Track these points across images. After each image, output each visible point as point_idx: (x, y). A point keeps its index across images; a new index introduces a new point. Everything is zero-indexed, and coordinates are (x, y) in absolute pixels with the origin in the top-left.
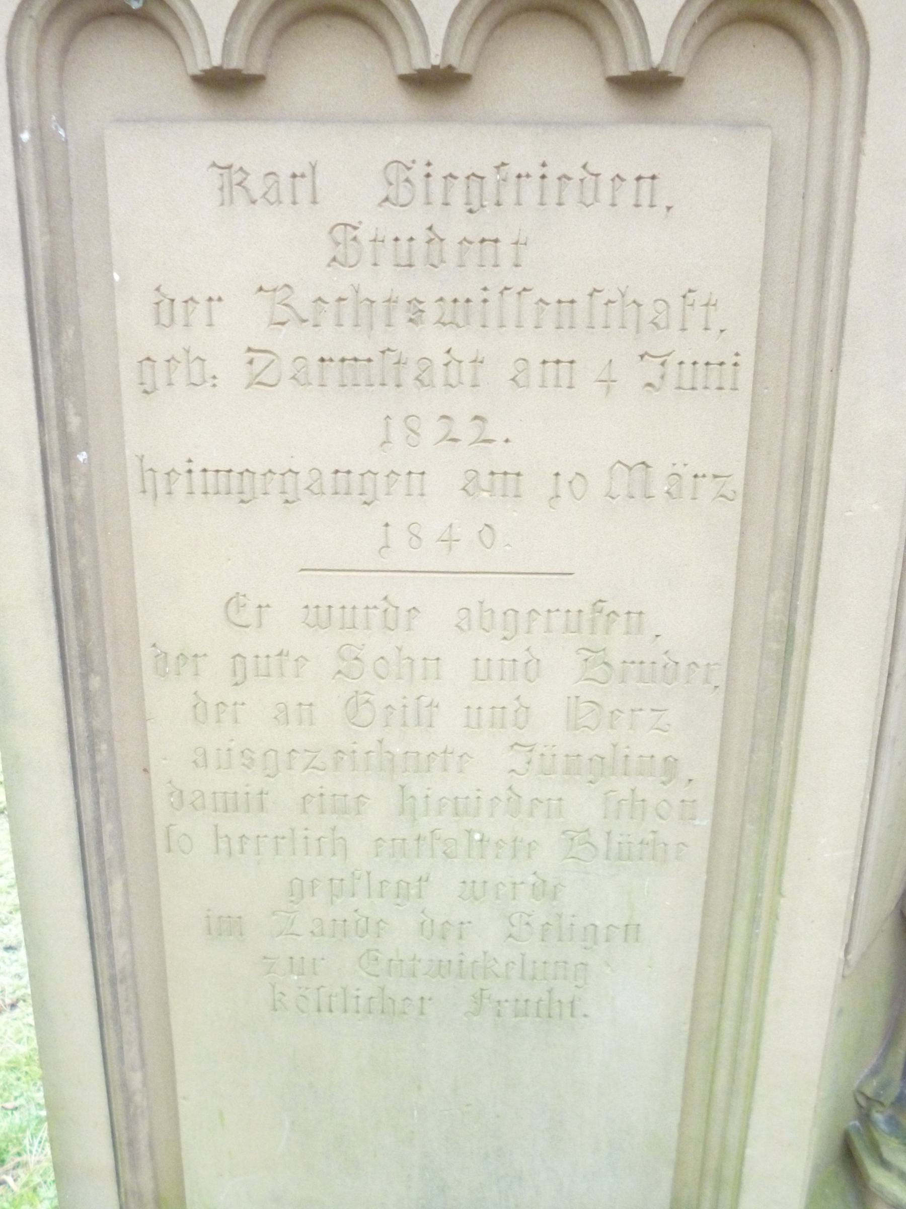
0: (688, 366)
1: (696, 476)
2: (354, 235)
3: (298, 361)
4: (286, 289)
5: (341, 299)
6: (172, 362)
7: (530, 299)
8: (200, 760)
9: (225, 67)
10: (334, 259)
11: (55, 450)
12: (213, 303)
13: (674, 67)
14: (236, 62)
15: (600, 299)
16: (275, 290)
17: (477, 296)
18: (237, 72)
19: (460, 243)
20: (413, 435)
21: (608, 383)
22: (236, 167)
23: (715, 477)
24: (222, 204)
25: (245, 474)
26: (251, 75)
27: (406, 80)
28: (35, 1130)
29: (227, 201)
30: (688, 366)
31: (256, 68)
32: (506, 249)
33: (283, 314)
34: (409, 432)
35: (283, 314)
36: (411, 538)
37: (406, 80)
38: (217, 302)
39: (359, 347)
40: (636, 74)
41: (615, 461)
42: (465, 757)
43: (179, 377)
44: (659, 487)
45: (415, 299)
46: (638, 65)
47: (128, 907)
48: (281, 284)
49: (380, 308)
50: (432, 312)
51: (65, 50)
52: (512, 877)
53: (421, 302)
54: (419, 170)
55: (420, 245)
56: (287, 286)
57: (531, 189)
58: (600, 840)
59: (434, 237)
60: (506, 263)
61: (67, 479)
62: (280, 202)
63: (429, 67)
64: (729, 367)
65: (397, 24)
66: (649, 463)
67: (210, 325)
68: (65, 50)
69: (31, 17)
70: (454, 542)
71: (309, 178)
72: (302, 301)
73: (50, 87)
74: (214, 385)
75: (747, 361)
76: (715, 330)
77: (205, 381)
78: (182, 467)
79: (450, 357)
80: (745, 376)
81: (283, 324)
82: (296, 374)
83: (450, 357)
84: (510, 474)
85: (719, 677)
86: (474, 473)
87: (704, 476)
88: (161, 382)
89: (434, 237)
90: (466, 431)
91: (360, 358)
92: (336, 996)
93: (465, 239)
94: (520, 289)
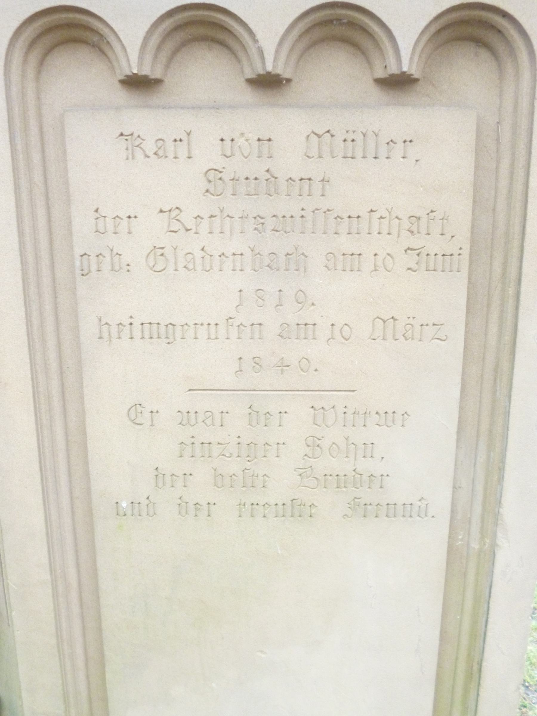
0: (432, 257)
1: (422, 325)
2: (219, 177)
3: (188, 255)
4: (177, 210)
5: (212, 216)
6: (100, 256)
9: (139, 74)
10: (207, 191)
12: (131, 219)
13: (415, 71)
14: (146, 71)
15: (376, 215)
16: (170, 211)
17: (297, 214)
18: (146, 77)
19: (287, 181)
20: (259, 300)
22: (136, 135)
23: (434, 325)
24: (127, 159)
25: (169, 326)
26: (143, 75)
27: (250, 81)
29: (130, 157)
30: (432, 257)
31: (157, 74)
32: (317, 186)
33: (175, 226)
34: (258, 298)
35: (175, 226)
37: (250, 81)
38: (134, 219)
40: (392, 76)
41: (375, 317)
42: (266, 506)
43: (106, 267)
45: (258, 216)
46: (393, 69)
48: (174, 207)
50: (270, 223)
51: (41, 63)
53: (262, 218)
56: (177, 208)
62: (166, 157)
63: (265, 73)
64: (455, 257)
65: (243, 46)
66: (396, 317)
67: (130, 233)
68: (41, 63)
70: (284, 368)
71: (185, 142)
73: (30, 86)
74: (128, 271)
75: (466, 252)
76: (448, 236)
77: (121, 268)
78: (126, 322)
81: (175, 232)
82: (187, 265)
84: (255, 324)
86: (410, 326)
87: (202, 324)
88: (94, 268)
91: (236, 253)
93: (290, 178)
94: (325, 210)
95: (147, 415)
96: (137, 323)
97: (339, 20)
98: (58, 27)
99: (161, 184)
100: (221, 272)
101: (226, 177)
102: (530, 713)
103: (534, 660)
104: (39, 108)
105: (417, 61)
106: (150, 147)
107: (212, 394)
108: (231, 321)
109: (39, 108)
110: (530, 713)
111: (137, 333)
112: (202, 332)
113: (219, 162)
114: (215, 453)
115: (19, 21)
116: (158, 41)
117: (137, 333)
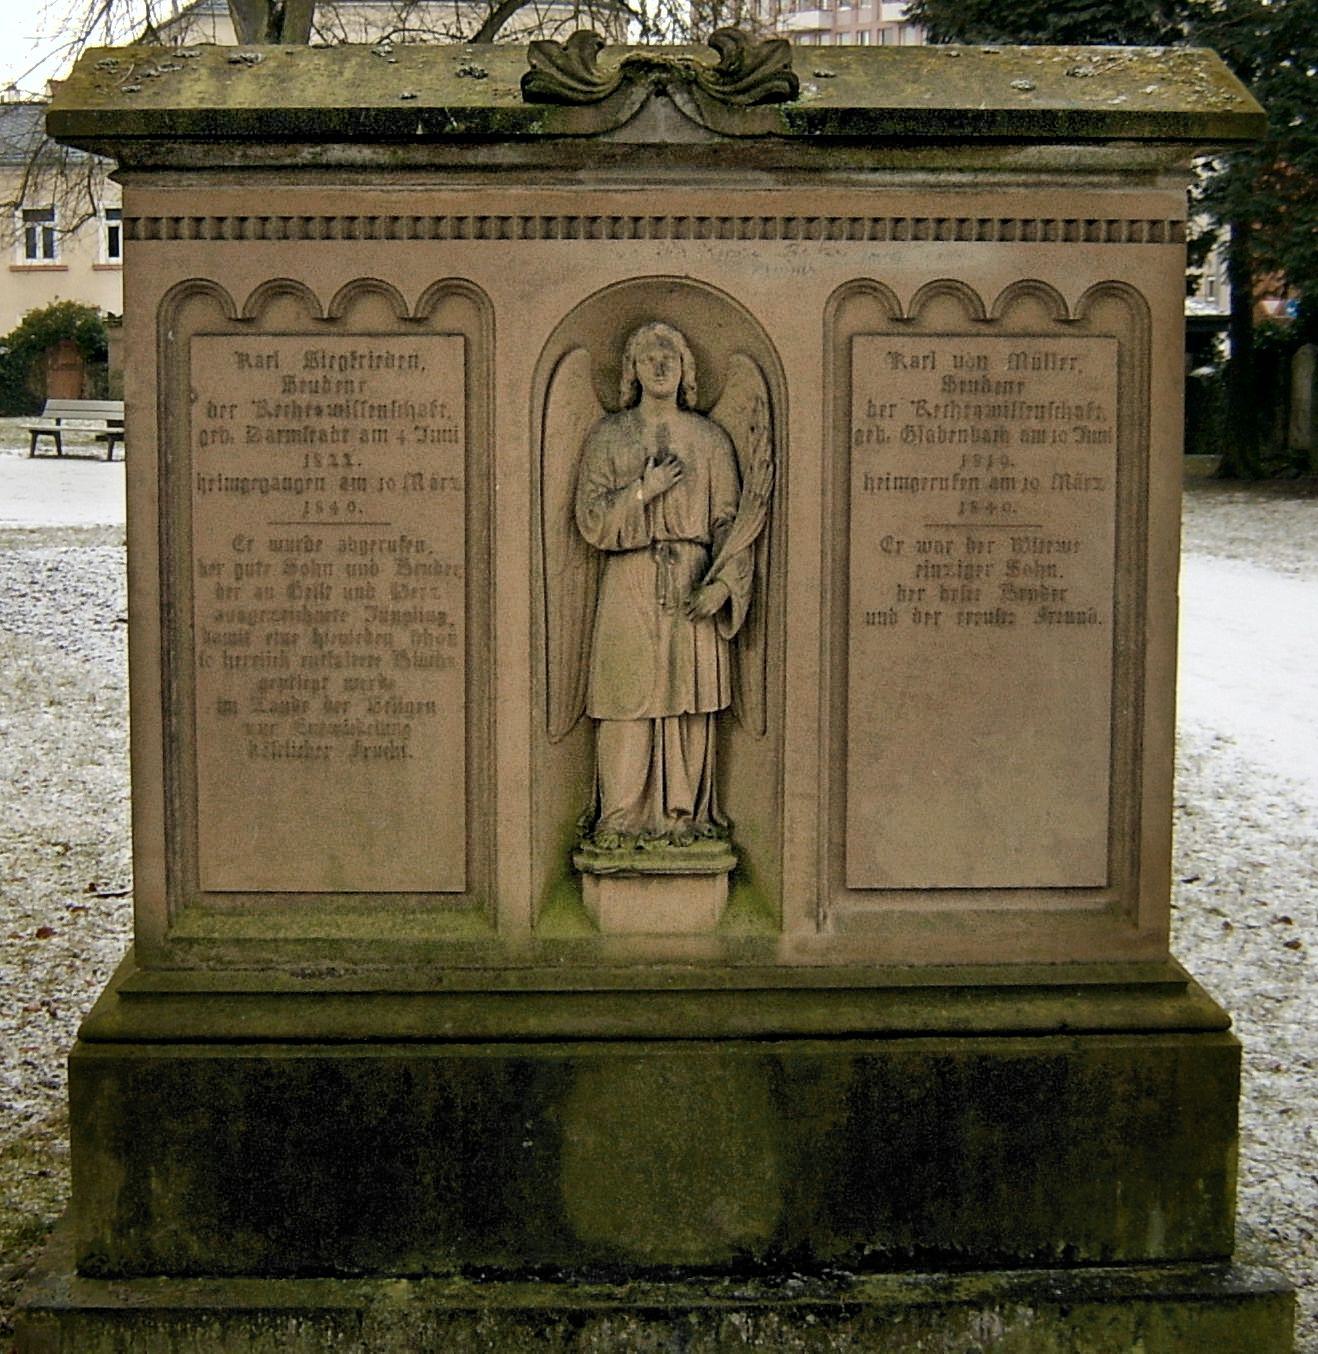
7: (367, 406)
8: (219, 617)
11: (402, 1053)
21: (402, 440)
28: (892, 118)
33: (262, 412)
36: (870, 619)
39: (295, 425)
43: (312, 486)
44: (426, 483)
47: (854, 184)
49: (876, 482)
50: (326, 411)
52: (1290, 1206)
54: (320, 355)
55: (321, 384)
57: (366, 362)
58: (410, 655)
59: (326, 380)
60: (357, 390)
61: (166, 482)
69: (395, 152)
72: (271, 407)
78: (215, 476)
79: (334, 430)
80: (461, 435)
83: (334, 430)
85: (462, 571)
89: (326, 380)
90: (341, 460)
92: (84, 960)
95: (895, 545)
96: (892, 477)
97: (450, 286)
98: (443, 288)
99: (691, 1109)
100: (350, 242)
101: (957, 381)
102: (137, 1350)
103: (1308, 1054)
104: (704, 766)
105: (1090, 907)
106: (908, 361)
107: (946, 916)
108: (975, 906)
109: (704, 766)
110: (137, 1350)
111: (892, 484)
112: (937, 484)
113: (953, 372)
114: (942, 573)
115: (1183, 720)
116: (1012, 150)
117: (892, 484)
